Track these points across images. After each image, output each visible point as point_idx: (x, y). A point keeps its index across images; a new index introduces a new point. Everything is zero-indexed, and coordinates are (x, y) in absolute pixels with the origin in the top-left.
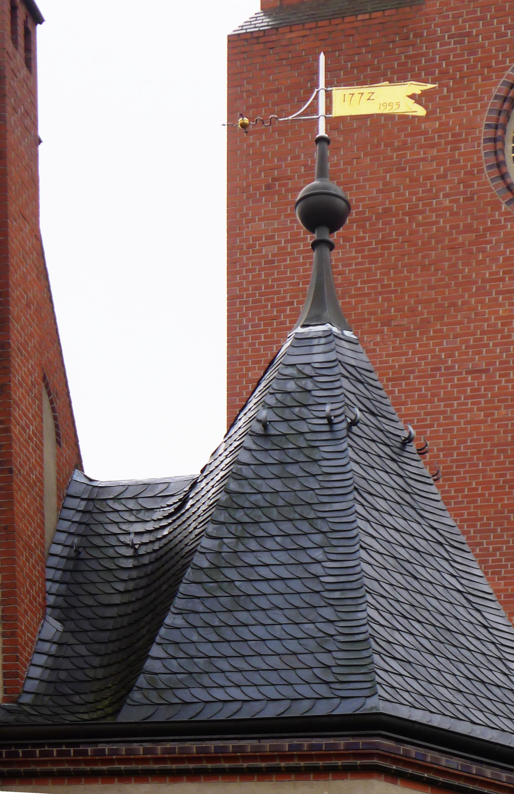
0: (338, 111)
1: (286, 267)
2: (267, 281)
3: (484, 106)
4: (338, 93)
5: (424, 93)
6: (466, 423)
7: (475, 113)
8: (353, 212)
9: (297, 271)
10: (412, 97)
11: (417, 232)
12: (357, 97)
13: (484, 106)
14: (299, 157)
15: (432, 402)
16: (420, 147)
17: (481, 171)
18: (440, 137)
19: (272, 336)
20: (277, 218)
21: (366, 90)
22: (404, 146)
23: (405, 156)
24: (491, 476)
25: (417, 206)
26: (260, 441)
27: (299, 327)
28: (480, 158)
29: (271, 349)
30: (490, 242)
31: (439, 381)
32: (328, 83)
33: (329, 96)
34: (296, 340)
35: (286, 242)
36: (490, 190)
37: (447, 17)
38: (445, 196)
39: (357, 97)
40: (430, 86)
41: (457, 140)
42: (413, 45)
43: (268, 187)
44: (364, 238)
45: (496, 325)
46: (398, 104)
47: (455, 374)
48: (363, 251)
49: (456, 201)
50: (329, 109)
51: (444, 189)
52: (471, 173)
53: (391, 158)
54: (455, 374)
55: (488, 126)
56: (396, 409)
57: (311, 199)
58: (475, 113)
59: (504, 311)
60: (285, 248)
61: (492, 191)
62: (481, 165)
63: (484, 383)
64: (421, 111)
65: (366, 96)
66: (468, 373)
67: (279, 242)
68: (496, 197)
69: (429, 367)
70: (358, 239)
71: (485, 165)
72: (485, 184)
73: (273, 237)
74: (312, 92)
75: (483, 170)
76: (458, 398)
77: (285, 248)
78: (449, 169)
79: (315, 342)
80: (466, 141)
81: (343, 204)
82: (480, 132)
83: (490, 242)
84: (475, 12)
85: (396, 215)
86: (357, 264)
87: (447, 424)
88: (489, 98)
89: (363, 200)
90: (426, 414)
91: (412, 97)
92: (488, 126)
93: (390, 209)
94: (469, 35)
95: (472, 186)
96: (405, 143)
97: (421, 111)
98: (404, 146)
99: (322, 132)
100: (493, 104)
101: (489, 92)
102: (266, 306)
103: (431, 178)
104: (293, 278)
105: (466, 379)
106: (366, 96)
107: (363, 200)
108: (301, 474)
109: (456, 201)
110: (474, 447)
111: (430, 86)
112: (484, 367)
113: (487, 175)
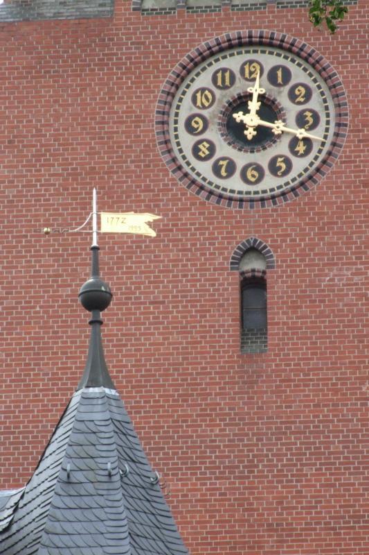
0: (104, 229)
1: (22, 206)
2: (8, 217)
3: (155, 97)
4: (104, 216)
5: (155, 221)
6: (150, 345)
7: (150, 102)
8: (114, 297)
9: (30, 211)
10: (149, 224)
11: (113, 188)
12: (115, 220)
13: (155, 97)
14: (31, 121)
15: (126, 325)
16: (114, 123)
17: (155, 146)
18: (127, 117)
19: (12, 262)
20: (16, 167)
21: (121, 215)
22: (103, 121)
23: (104, 128)
24: (169, 391)
25: (112, 167)
26: (64, 486)
27: (84, 388)
28: (153, 136)
29: (67, 395)
30: (162, 200)
31: (131, 309)
32: (100, 209)
33: (99, 218)
34: (83, 399)
35: (23, 186)
36: (161, 160)
37: (129, 29)
38: (132, 162)
39: (115, 220)
40: (158, 217)
41: (138, 120)
42: (108, 46)
43: (10, 142)
44: (77, 189)
45: (168, 266)
46: (139, 227)
47: (141, 303)
48: (76, 199)
49: (139, 167)
50: (99, 228)
51: (130, 156)
52: (148, 146)
53: (95, 128)
54: (141, 303)
55: (158, 112)
56: (137, 432)
57: (90, 293)
58: (150, 102)
59: (173, 256)
60: (22, 191)
61: (162, 161)
62: (154, 141)
63: (161, 313)
64: (153, 234)
65: (121, 220)
66: (151, 303)
67: (18, 186)
68: (165, 166)
69: (124, 296)
70: (73, 189)
71: (157, 141)
72: (158, 155)
73: (13, 182)
74: (89, 215)
75: (155, 144)
76: (145, 324)
77: (22, 191)
78: (134, 142)
79: (95, 402)
80: (144, 121)
81: (108, 295)
82: (153, 116)
83: (162, 200)
84: (147, 28)
85: (99, 173)
86: (72, 209)
87: (137, 345)
88: (158, 92)
89: (76, 159)
90: (122, 335)
91: (149, 224)
92: (158, 112)
93: (95, 168)
94: (144, 43)
95: (149, 156)
96: (104, 118)
97: (153, 234)
98: (103, 121)
99: (95, 244)
100: (161, 97)
101: (158, 87)
102: (8, 237)
103: (122, 147)
104: (27, 216)
105: (149, 308)
106: (121, 220)
107: (76, 159)
108: (94, 518)
109: (139, 167)
110: (157, 365)
111: (158, 217)
112: (161, 299)
113: (159, 149)
